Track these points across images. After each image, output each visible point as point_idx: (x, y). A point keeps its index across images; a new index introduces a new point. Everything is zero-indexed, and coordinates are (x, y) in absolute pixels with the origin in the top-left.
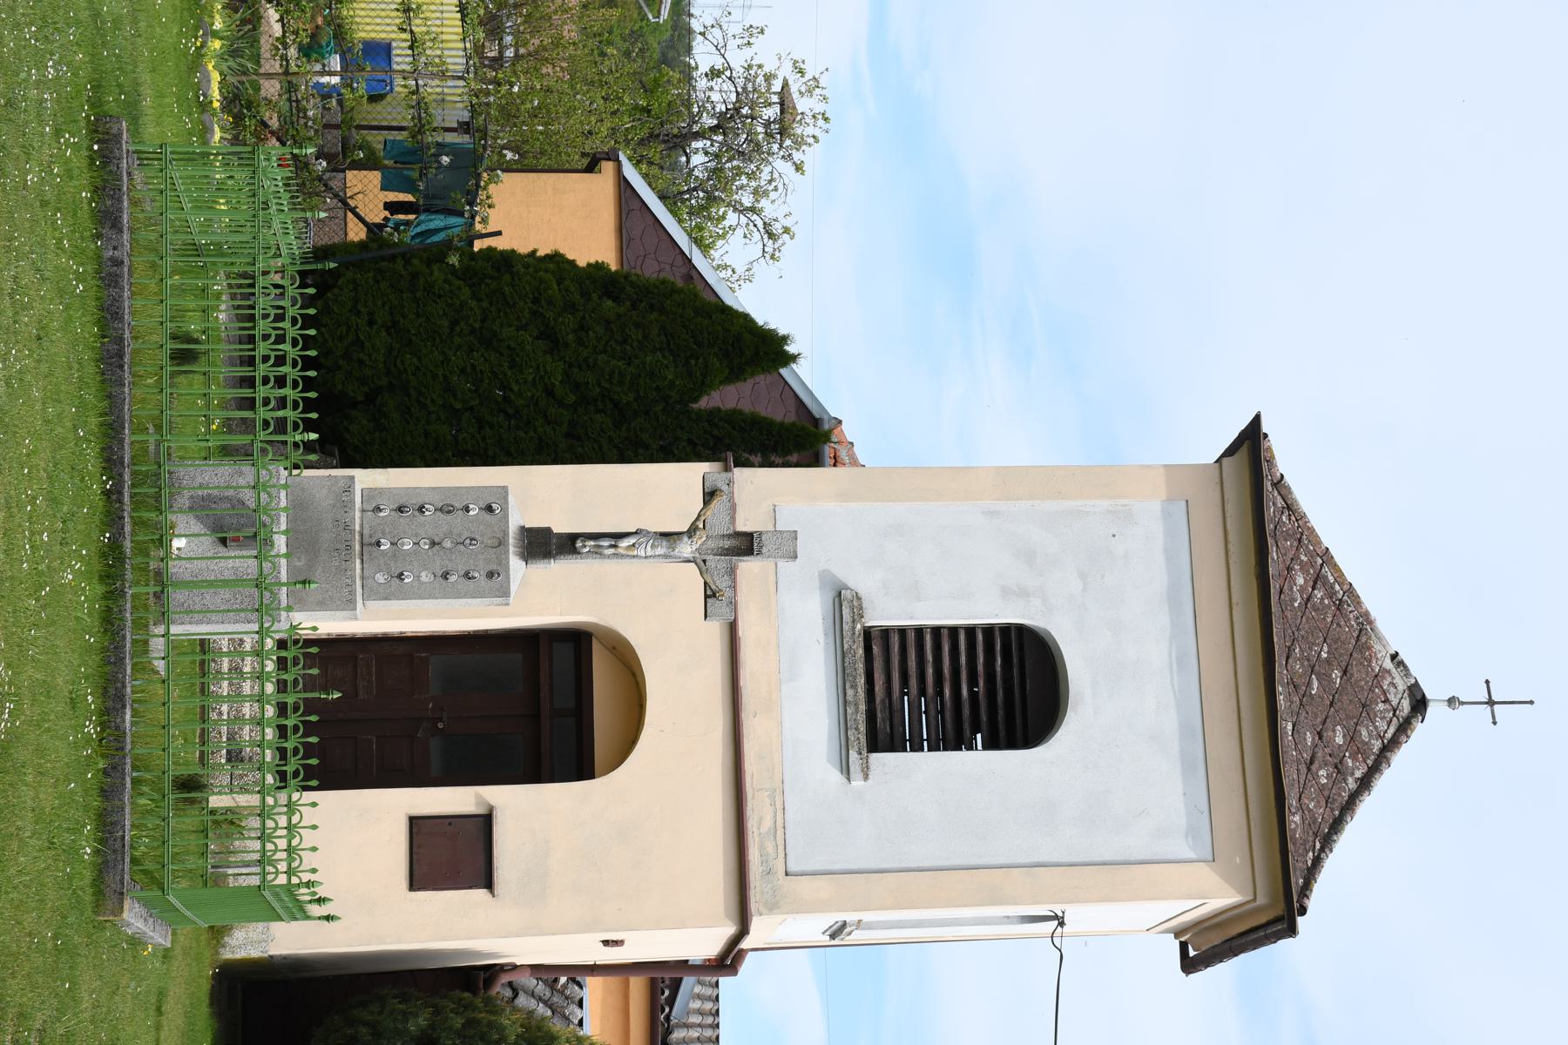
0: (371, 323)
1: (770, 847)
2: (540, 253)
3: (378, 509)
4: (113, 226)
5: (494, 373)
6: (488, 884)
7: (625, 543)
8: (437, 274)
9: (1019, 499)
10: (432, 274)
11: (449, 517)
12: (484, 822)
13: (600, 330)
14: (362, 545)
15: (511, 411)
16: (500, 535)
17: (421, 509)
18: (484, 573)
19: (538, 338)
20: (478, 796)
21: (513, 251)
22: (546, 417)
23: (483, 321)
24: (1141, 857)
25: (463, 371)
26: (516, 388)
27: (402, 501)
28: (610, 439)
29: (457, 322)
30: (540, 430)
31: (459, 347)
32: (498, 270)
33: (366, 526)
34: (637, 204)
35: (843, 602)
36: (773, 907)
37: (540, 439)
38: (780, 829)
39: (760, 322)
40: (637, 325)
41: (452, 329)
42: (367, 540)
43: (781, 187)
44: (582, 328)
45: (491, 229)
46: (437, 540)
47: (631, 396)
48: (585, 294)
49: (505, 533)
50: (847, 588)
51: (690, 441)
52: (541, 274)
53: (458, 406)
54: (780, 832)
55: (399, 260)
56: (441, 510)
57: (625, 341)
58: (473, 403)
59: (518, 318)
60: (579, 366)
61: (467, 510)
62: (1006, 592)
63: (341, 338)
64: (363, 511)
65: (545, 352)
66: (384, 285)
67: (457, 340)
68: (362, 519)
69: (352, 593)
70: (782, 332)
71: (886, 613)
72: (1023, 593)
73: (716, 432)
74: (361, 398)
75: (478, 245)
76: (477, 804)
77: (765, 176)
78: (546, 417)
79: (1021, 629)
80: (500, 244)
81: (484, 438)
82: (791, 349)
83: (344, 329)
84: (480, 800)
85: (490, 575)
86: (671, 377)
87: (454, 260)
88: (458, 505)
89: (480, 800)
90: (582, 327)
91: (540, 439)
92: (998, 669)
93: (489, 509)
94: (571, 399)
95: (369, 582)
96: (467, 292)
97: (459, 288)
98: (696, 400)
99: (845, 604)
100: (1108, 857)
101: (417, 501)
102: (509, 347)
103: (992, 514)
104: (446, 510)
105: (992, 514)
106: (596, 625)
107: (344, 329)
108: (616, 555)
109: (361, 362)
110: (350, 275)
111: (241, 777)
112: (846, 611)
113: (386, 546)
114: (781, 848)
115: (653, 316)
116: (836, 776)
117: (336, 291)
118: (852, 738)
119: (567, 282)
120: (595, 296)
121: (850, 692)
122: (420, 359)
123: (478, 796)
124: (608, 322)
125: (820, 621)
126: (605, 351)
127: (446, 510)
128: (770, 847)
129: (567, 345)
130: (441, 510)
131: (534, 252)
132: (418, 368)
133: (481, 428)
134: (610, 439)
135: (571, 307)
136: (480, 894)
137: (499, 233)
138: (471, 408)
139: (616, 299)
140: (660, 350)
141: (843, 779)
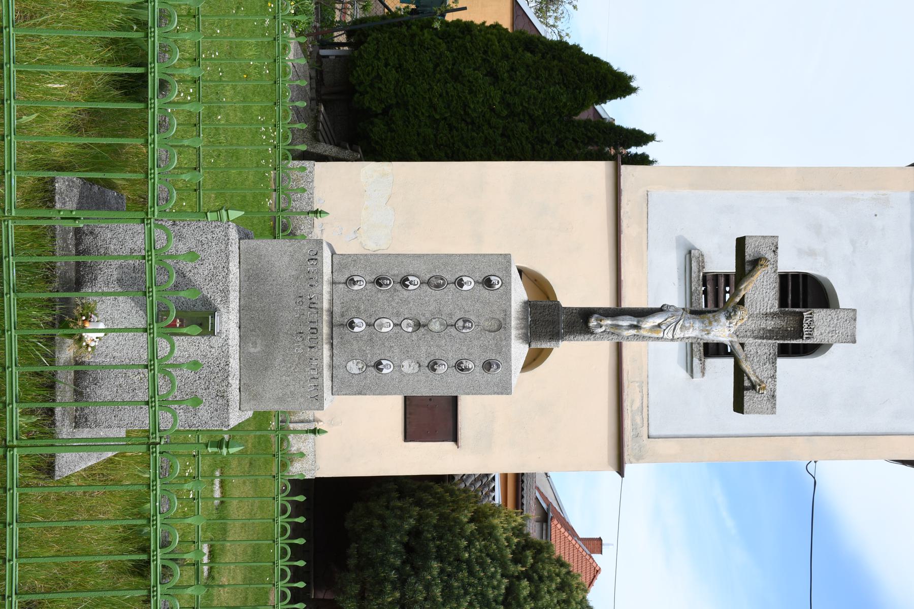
0: (386, 65)
1: (638, 419)
2: (487, 24)
3: (351, 281)
5: (460, 97)
6: (455, 439)
7: (649, 323)
8: (427, 34)
9: (813, 189)
10: (423, 35)
11: (438, 293)
13: (523, 71)
14: (332, 325)
15: (469, 120)
16: (500, 316)
17: (404, 282)
18: (479, 363)
19: (486, 75)
22: (489, 124)
23: (454, 65)
25: (441, 95)
26: (472, 106)
27: (381, 271)
28: (527, 138)
29: (436, 65)
30: (486, 132)
31: (439, 81)
32: (463, 33)
33: (337, 302)
34: (521, 13)
36: (639, 458)
37: (486, 138)
38: (644, 408)
39: (615, 68)
40: (545, 68)
41: (435, 69)
42: (337, 319)
43: (567, 17)
44: (512, 69)
45: (459, 6)
46: (423, 320)
47: (541, 112)
48: (514, 49)
49: (506, 313)
50: (695, 249)
51: (574, 140)
52: (489, 36)
53: (437, 117)
54: (645, 410)
55: (404, 26)
56: (428, 283)
57: (538, 78)
58: (447, 115)
59: (474, 63)
60: (510, 93)
61: (460, 283)
63: (368, 75)
64: (333, 283)
65: (490, 84)
66: (395, 41)
67: (438, 76)
68: (332, 294)
69: (319, 387)
70: (629, 73)
72: (812, 253)
73: (589, 134)
74: (379, 111)
75: (450, 17)
77: (560, 11)
78: (489, 124)
79: (806, 276)
80: (464, 16)
81: (452, 137)
82: (634, 84)
83: (370, 68)
85: (488, 366)
86: (564, 100)
87: (437, 25)
88: (450, 277)
90: (513, 69)
91: (486, 138)
93: (488, 283)
94: (505, 113)
95: (339, 372)
96: (444, 46)
97: (440, 44)
98: (576, 114)
99: (693, 259)
100: (861, 431)
101: (398, 272)
102: (469, 81)
103: (794, 199)
104: (435, 283)
105: (794, 199)
106: (526, 268)
107: (370, 68)
108: (636, 337)
109: (380, 89)
110: (374, 35)
112: (694, 264)
113: (360, 327)
114: (645, 420)
115: (556, 62)
116: (683, 374)
117: (366, 45)
118: (695, 349)
119: (504, 41)
120: (520, 50)
122: (415, 88)
124: (528, 66)
126: (526, 84)
127: (435, 283)
128: (638, 419)
129: (503, 80)
130: (428, 283)
131: (484, 23)
132: (414, 94)
133: (451, 130)
134: (527, 138)
135: (506, 57)
136: (450, 445)
137: (465, 8)
138: (445, 119)
139: (532, 52)
140: (559, 84)
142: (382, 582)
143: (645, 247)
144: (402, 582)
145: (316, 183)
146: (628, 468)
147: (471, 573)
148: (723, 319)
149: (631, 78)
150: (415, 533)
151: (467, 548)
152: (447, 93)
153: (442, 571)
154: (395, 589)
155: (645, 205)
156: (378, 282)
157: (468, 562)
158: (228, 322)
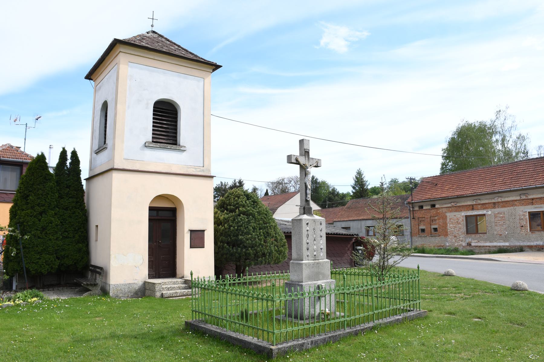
0: (39, 259)
1: (198, 170)
4: (303, 346)
6: (204, 231)
12: (192, 231)
21: (375, 187)
35: (146, 146)
36: (209, 171)
38: (195, 167)
40: (38, 191)
71: (149, 136)
72: (147, 104)
82: (40, 154)
84: (187, 233)
89: (187, 233)
113: (315, 253)
116: (185, 153)
128: (198, 170)
142: (246, 254)
144: (245, 247)
145: (118, 283)
146: (212, 175)
147: (241, 226)
148: (308, 169)
150: (228, 243)
151: (234, 227)
153: (241, 235)
154: (248, 250)
156: (308, 249)
158: (319, 282)
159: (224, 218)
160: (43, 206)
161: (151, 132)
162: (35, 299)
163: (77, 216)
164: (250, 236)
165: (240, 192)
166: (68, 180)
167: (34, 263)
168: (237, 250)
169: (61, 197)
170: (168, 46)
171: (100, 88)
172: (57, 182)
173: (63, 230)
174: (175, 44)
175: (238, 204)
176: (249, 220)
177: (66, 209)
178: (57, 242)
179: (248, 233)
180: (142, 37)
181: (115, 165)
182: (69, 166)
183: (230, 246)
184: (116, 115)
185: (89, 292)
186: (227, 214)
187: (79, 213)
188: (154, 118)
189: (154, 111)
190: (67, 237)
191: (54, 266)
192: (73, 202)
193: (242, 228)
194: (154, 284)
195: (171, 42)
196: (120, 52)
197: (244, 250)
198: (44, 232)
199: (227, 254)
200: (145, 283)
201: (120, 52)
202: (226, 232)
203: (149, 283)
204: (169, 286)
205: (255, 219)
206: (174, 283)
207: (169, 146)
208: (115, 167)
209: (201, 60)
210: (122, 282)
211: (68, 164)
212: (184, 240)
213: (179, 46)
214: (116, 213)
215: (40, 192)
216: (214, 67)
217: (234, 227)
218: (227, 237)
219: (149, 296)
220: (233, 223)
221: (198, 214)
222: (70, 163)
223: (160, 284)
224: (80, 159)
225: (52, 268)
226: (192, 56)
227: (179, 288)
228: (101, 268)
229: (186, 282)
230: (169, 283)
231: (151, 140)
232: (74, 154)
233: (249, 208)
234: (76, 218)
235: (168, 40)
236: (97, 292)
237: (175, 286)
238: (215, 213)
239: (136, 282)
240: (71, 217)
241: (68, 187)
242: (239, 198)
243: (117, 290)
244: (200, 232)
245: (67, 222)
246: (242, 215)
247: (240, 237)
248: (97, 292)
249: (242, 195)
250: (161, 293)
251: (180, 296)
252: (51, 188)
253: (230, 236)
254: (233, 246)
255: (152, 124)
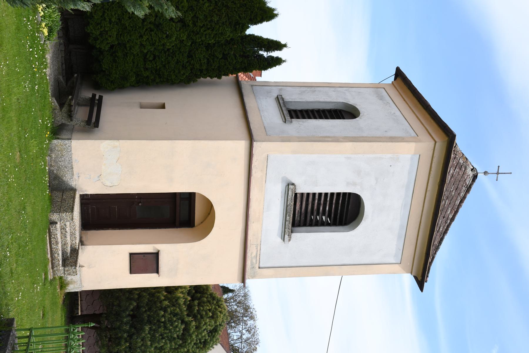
1: (254, 261)
6: (157, 272)
12: (156, 255)
20: (154, 247)
24: (377, 262)
36: (253, 277)
38: (258, 257)
40: (217, 15)
62: (348, 184)
71: (303, 188)
72: (354, 184)
76: (154, 249)
82: (275, 12)
84: (154, 248)
89: (154, 248)
92: (340, 202)
111: (68, 271)
116: (279, 240)
118: (286, 231)
121: (288, 218)
123: (154, 247)
125: (280, 194)
128: (254, 261)
136: (155, 275)
141: (282, 241)
143: (264, 182)
144: (130, 336)
145: (73, 152)
147: (166, 328)
149: (274, 10)
150: (138, 307)
152: (152, 39)
153: (151, 329)
154: (126, 341)
155: (266, 162)
157: (164, 323)
159: (179, 298)
160: (194, 24)
161: (311, 191)
162: (46, 31)
163: (179, 72)
164: (149, 343)
165: (220, 320)
166: (235, 56)
167: (104, 14)
168: (126, 324)
169: (208, 47)
170: (452, 205)
171: (381, 98)
172: (232, 39)
173: (157, 54)
174: (456, 212)
175: (202, 317)
176: (174, 338)
177: (190, 56)
178: (137, 47)
179: (153, 340)
180: (463, 166)
181: (259, 143)
182: (260, 55)
183: (132, 310)
184: (336, 140)
185: (58, 107)
186: (184, 304)
187: (184, 74)
188: (332, 194)
189: (345, 194)
190: (145, 59)
191: (98, 42)
192: (201, 65)
193: (161, 330)
194: (72, 210)
195: (460, 205)
196: (436, 142)
197: (125, 335)
198: (152, 27)
199: (119, 305)
200: (74, 190)
201: (436, 142)
202: (155, 303)
203: (74, 198)
204: (68, 229)
205: (178, 348)
206: (72, 234)
207: (290, 218)
208: (255, 143)
209: (430, 260)
210: (74, 157)
211: (261, 52)
212: (143, 242)
213: (452, 219)
214: (184, 147)
215: (216, 19)
216: (420, 278)
217: (163, 316)
218: (147, 305)
219: (52, 200)
220: (170, 314)
221: (184, 263)
222: (262, 55)
223: (72, 219)
224: (275, 39)
225: (96, 39)
226: (436, 243)
227: (64, 244)
228: (97, 125)
229: (75, 252)
230: (73, 227)
231: (299, 191)
232: (278, 61)
233: (194, 337)
234: (177, 72)
235: (462, 201)
236: (58, 119)
237: (68, 238)
238: (185, 287)
239: (75, 177)
240: (177, 63)
241: (225, 57)
242: (212, 317)
243: (61, 151)
244: (155, 262)
245: (170, 58)
246: (183, 327)
247: (147, 328)
248: (58, 119)
249: (216, 322)
250: (56, 220)
251: (51, 251)
252: (222, 33)
253: (150, 309)
254: (133, 316)
255: (323, 191)
